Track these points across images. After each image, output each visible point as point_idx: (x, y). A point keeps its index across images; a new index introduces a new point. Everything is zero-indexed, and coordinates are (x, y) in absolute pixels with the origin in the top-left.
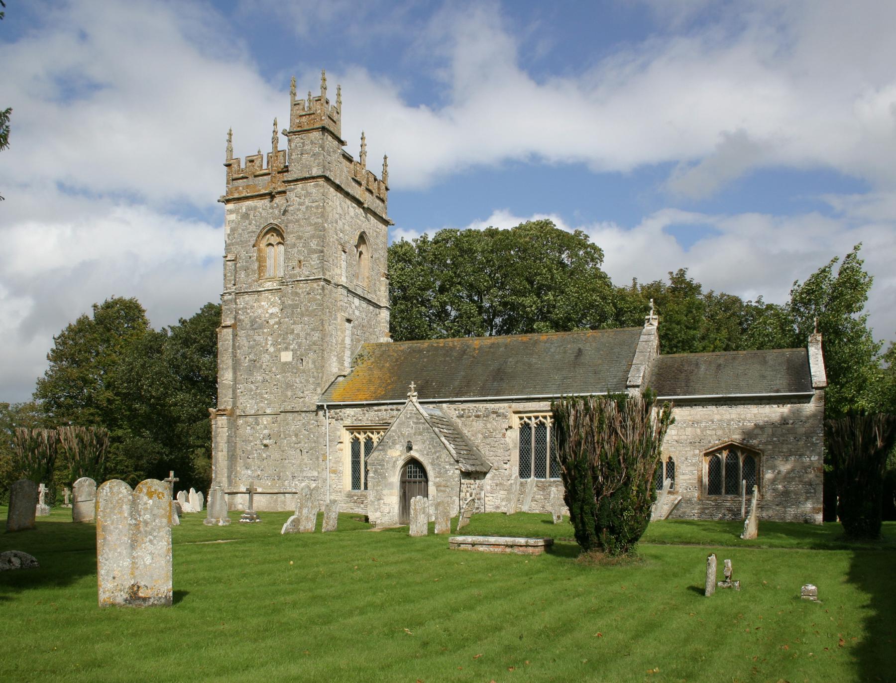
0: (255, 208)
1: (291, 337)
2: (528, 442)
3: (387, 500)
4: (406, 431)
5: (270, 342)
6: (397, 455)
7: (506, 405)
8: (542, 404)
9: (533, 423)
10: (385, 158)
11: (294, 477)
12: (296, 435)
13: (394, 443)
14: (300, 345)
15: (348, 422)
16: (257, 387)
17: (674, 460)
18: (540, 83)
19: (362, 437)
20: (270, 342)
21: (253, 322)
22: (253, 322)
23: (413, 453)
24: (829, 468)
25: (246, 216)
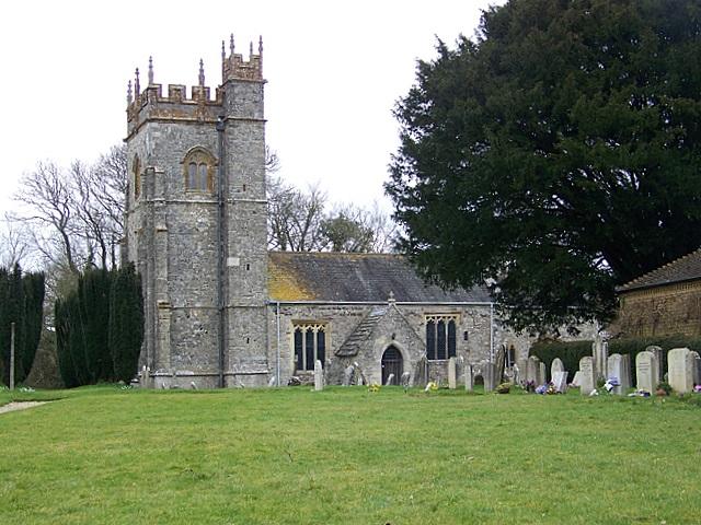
0: (181, 131)
1: (238, 246)
2: (433, 335)
3: (375, 375)
4: (390, 326)
5: (199, 247)
6: (382, 343)
7: (420, 308)
8: (446, 308)
9: (437, 322)
10: (202, 64)
11: (242, 361)
12: (244, 327)
13: (380, 335)
14: (247, 253)
15: (296, 317)
16: (187, 285)
17: (515, 347)
18: (409, 111)
19: (304, 330)
20: (199, 247)
21: (181, 228)
22: (181, 228)
23: (396, 343)
24: (506, 11)
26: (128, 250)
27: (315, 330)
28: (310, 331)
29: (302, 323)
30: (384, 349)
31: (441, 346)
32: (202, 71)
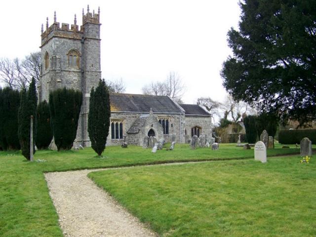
23: (153, 128)
25: (63, 44)
26: (41, 91)
27: (119, 123)
28: (117, 124)
29: (116, 120)
30: (149, 130)
31: (117, 134)
32: (55, 15)
